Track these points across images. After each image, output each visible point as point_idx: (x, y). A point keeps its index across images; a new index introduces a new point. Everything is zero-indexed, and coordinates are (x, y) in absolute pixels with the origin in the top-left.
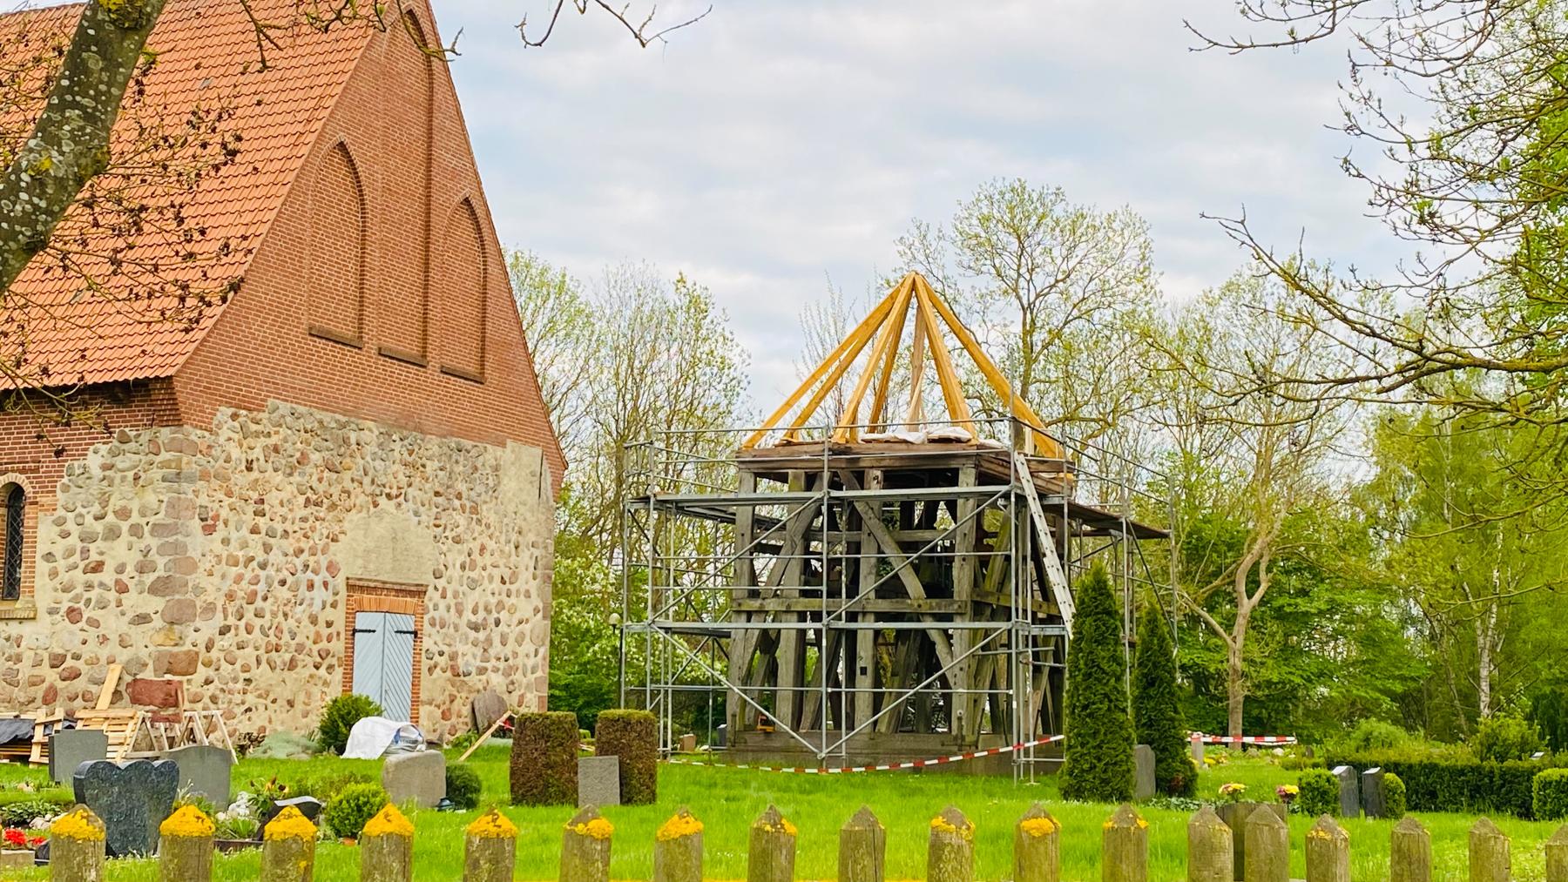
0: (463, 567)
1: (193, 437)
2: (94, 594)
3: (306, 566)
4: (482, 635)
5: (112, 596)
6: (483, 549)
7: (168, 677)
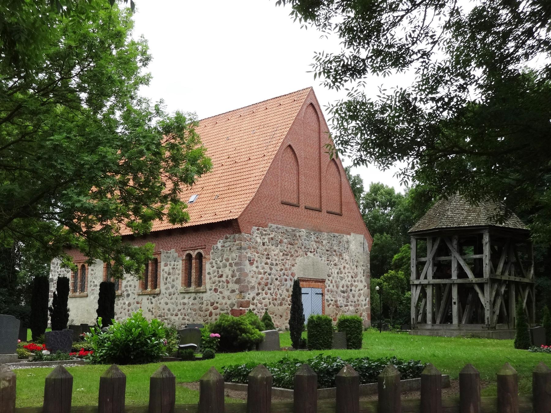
1: (245, 236)
2: (220, 284)
3: (284, 274)
5: (225, 284)
6: (344, 267)
7: (241, 308)
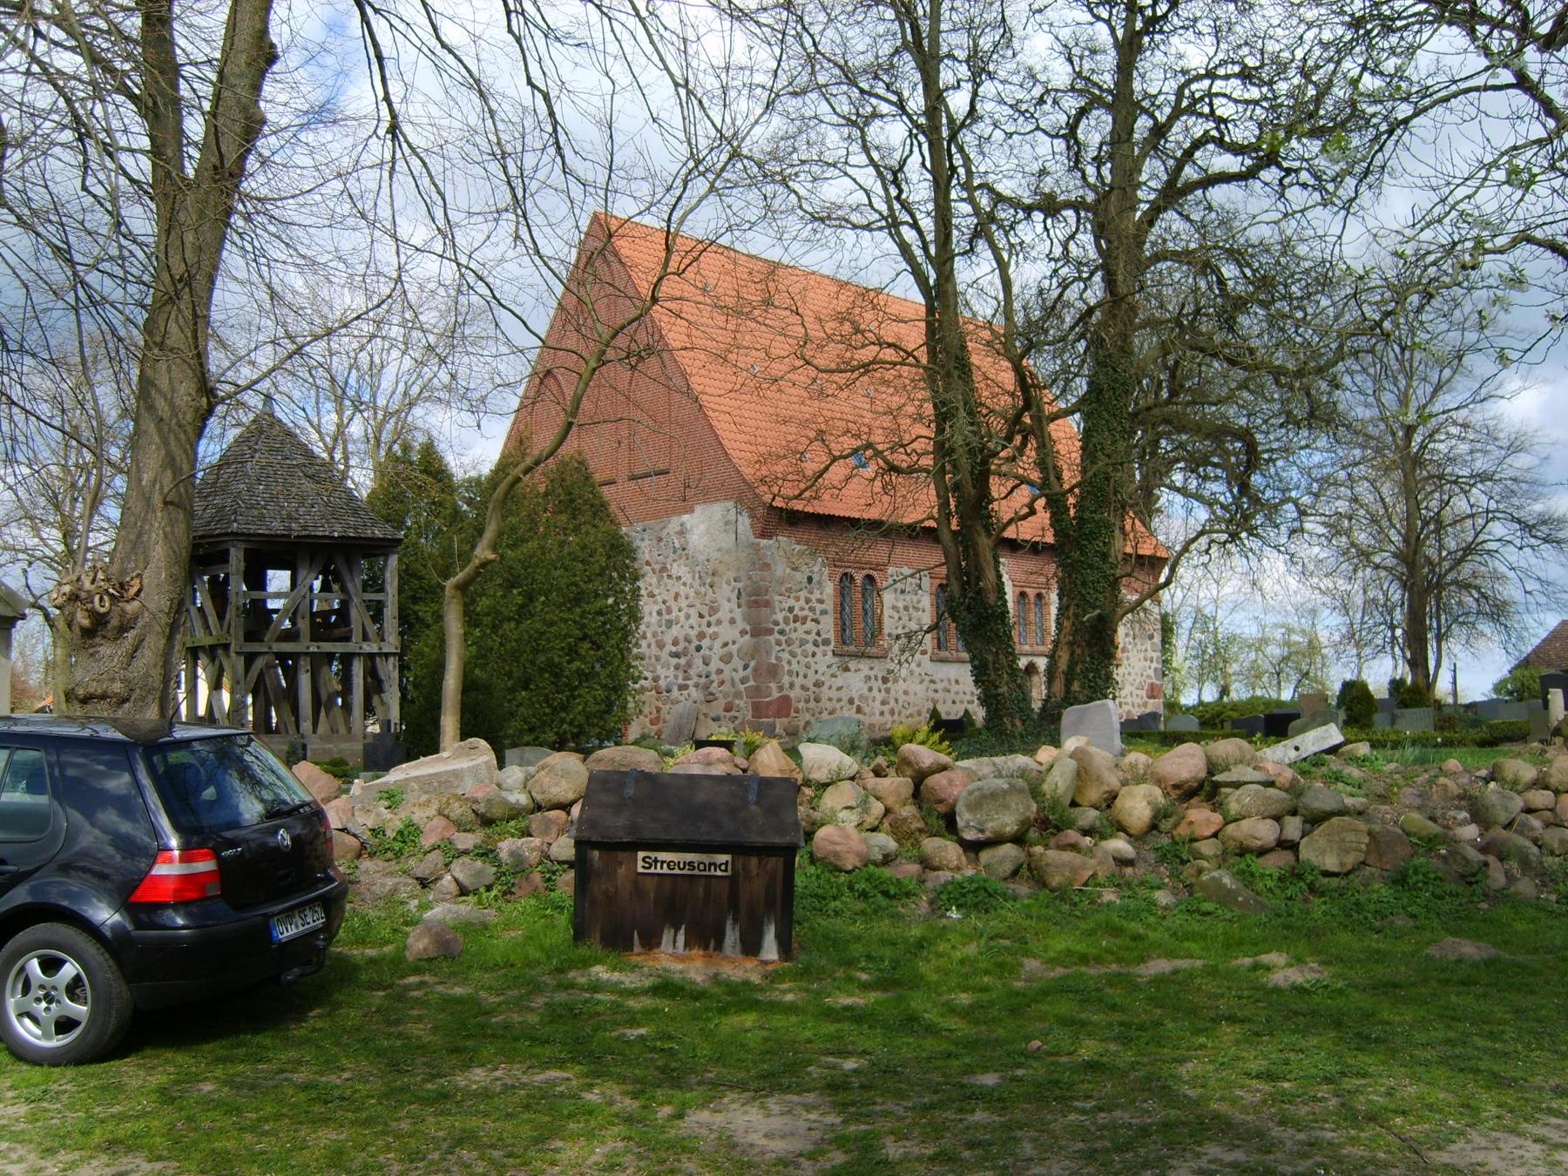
0: (659, 613)
4: (683, 661)
